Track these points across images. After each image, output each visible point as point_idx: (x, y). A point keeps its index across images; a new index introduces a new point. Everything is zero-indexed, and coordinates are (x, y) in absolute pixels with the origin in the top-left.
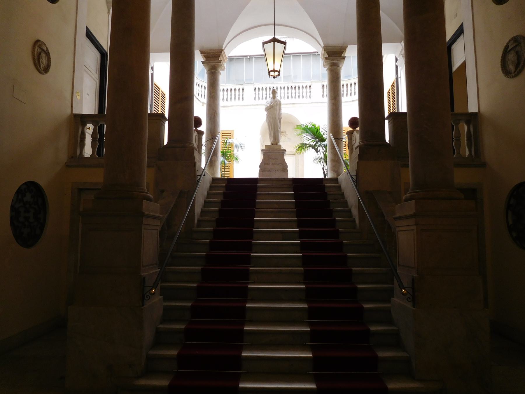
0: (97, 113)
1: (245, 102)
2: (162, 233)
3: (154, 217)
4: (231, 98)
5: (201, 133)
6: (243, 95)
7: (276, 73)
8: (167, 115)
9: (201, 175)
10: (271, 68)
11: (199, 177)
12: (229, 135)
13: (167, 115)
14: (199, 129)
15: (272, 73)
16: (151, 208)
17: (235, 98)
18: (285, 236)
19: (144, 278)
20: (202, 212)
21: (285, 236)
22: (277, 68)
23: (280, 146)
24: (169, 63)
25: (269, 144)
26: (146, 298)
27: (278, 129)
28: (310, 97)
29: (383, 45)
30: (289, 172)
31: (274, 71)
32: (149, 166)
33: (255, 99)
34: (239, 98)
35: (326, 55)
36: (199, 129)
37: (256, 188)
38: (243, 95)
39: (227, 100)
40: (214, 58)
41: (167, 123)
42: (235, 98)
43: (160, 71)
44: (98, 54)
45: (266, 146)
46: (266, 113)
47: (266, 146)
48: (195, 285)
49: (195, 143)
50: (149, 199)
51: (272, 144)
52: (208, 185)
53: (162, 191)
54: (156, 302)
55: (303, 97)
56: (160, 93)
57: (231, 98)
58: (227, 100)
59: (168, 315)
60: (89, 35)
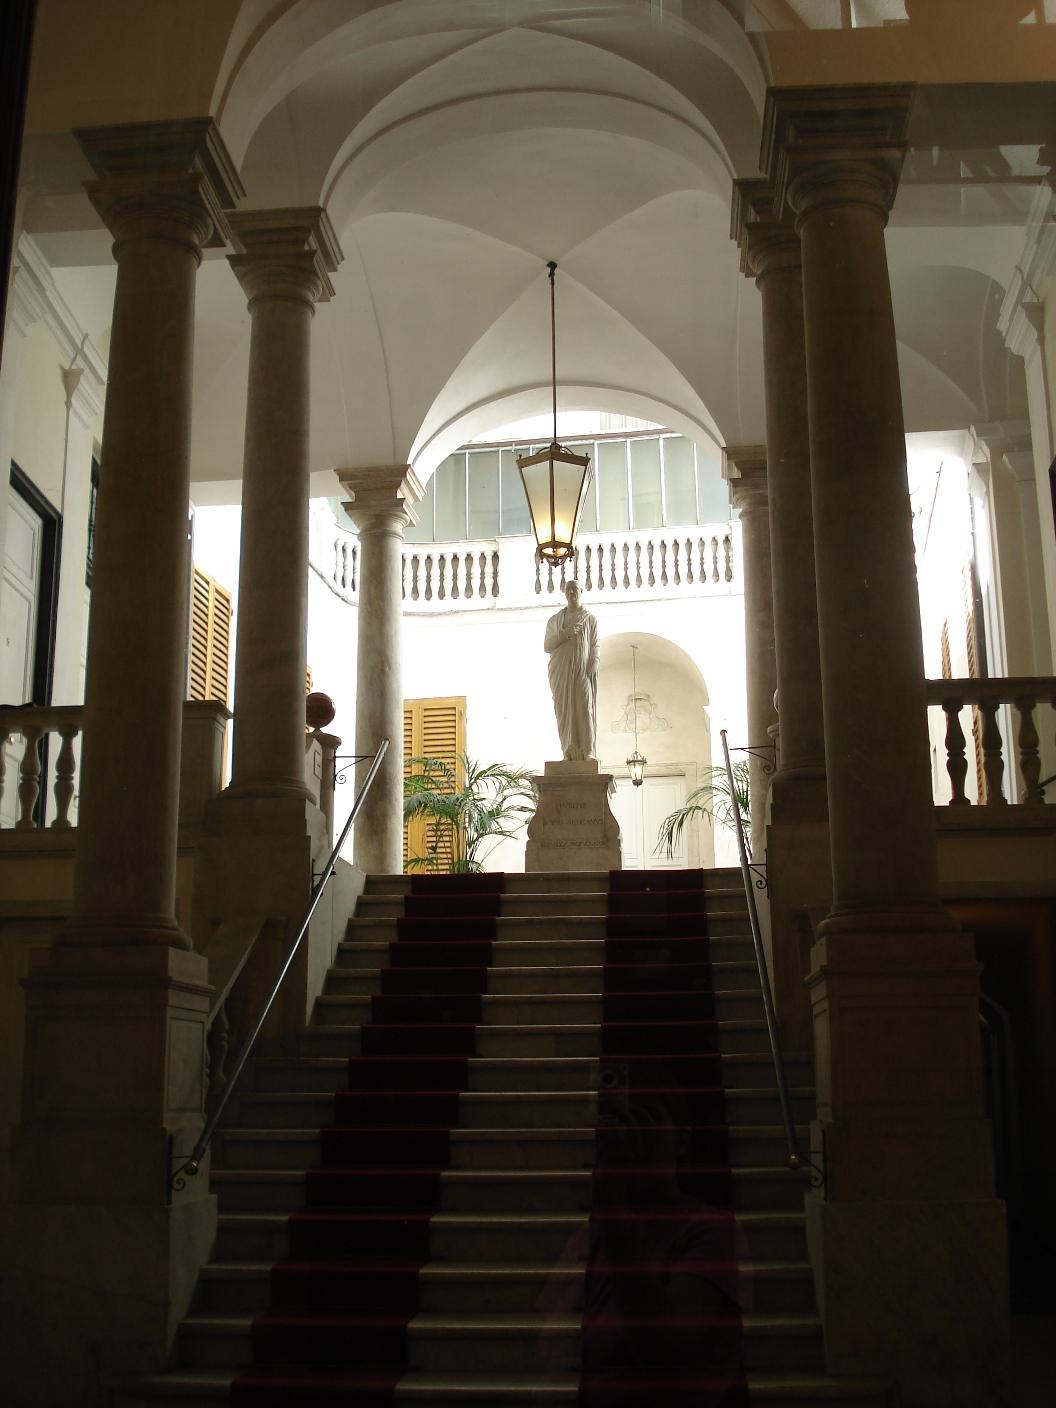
0: (28, 700)
1: (502, 600)
2: (213, 1039)
3: (193, 990)
4: (455, 589)
5: (331, 743)
6: (495, 574)
7: (562, 551)
8: (231, 707)
9: (324, 874)
10: (545, 537)
11: (317, 879)
12: (446, 717)
13: (231, 707)
14: (325, 730)
15: (549, 551)
16: (187, 965)
17: (469, 588)
18: (564, 1041)
19: (171, 1139)
20: (331, 981)
21: (564, 1041)
22: (563, 536)
23: (595, 763)
24: (239, 508)
25: (558, 756)
26: (176, 1186)
27: (585, 706)
28: (495, 590)
29: (907, 435)
30: (625, 847)
31: (555, 544)
32: (183, 851)
33: (538, 589)
34: (482, 587)
35: (737, 474)
36: (325, 730)
37: (496, 907)
38: (495, 574)
39: (442, 595)
40: (376, 497)
41: (230, 722)
42: (469, 588)
43: (215, 537)
44: (36, 522)
45: (547, 764)
46: (548, 657)
47: (547, 764)
48: (302, 1173)
49: (310, 780)
50: (182, 946)
51: (568, 754)
52: (348, 907)
53: (216, 923)
54: (196, 1203)
55: (703, 577)
56: (212, 596)
57: (455, 589)
58: (442, 595)
59: (229, 1242)
60: (21, 483)
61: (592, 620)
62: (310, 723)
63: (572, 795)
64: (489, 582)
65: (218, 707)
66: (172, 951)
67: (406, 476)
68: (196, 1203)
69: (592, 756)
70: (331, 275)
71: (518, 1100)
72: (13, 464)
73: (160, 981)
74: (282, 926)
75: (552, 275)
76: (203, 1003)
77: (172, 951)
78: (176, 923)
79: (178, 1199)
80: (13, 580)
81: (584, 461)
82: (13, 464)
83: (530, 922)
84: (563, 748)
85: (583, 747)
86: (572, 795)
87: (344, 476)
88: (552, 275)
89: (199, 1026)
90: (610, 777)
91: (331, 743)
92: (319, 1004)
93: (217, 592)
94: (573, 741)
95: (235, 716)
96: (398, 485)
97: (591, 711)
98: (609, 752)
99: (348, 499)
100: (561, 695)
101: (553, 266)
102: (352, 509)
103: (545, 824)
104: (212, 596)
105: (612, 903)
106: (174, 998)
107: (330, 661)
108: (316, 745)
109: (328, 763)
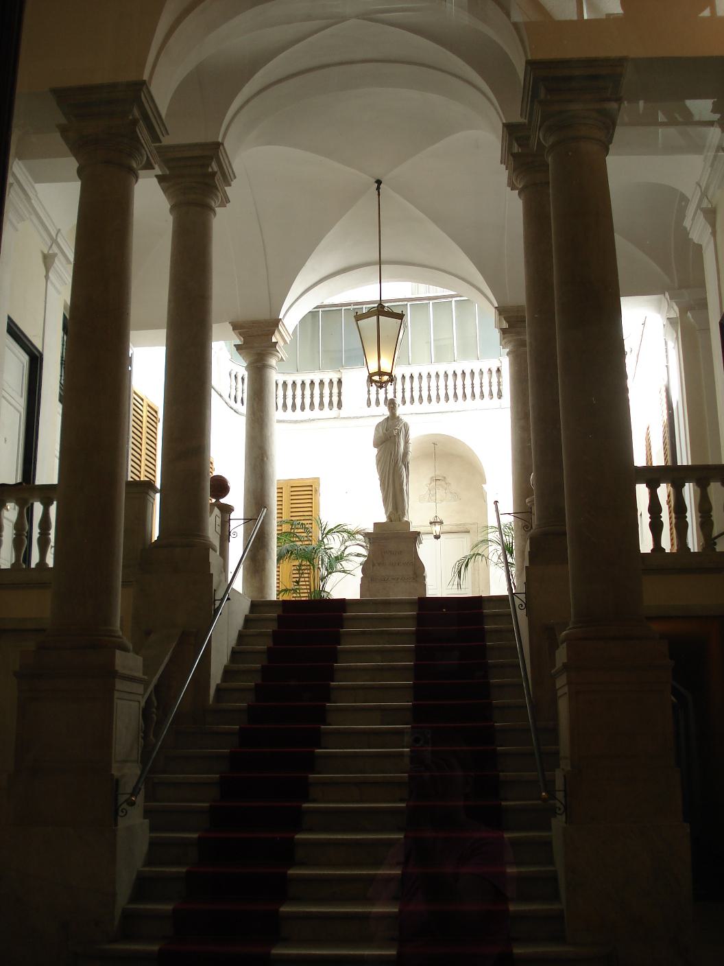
1: (344, 412)
2: (146, 713)
3: (132, 679)
4: (312, 404)
5: (227, 510)
6: (340, 394)
7: (386, 378)
8: (158, 485)
9: (222, 600)
10: (374, 369)
11: (217, 603)
12: (306, 492)
13: (158, 485)
14: (223, 501)
15: (376, 378)
16: (128, 662)
17: (321, 404)
18: (387, 714)
19: (117, 781)
20: (227, 673)
21: (387, 714)
22: (386, 368)
23: (408, 523)
24: (164, 348)
25: (383, 519)
26: (121, 814)
27: (401, 485)
28: (340, 405)
29: (622, 299)
30: (428, 581)
31: (380, 373)
32: (125, 584)
33: (369, 404)
34: (331, 403)
35: (505, 325)
36: (223, 501)
37: (340, 622)
38: (340, 394)
39: (303, 408)
40: (258, 341)
41: (158, 495)
42: (321, 404)
43: (147, 368)
44: (25, 358)
45: (375, 524)
46: (375, 451)
47: (375, 524)
48: (207, 805)
49: (213, 535)
50: (125, 649)
51: (389, 517)
53: (148, 633)
54: (134, 825)
55: (482, 396)
56: (145, 409)
57: (312, 404)
58: (303, 408)
59: (157, 852)
60: (14, 332)
61: (406, 426)
62: (213, 496)
63: (392, 546)
64: (335, 399)
65: (149, 485)
66: (118, 652)
67: (278, 327)
68: (134, 825)
69: (406, 519)
70: (227, 188)
71: (355, 755)
72: (9, 318)
73: (109, 673)
74: (194, 635)
75: (378, 188)
76: (139, 688)
77: (118, 652)
78: (120, 633)
79: (122, 823)
80: (9, 398)
81: (400, 316)
82: (9, 318)
83: (363, 633)
84: (386, 513)
85: (400, 513)
86: (392, 546)
87: (236, 327)
88: (378, 188)
89: (137, 704)
90: (418, 533)
91: (227, 510)
92: (218, 689)
93: (149, 406)
94: (393, 508)
95: (161, 491)
96: (273, 333)
97: (405, 488)
98: (417, 516)
99: (238, 342)
100: (385, 477)
101: (379, 182)
102: (241, 349)
103: (374, 565)
104: (145, 409)
105: (420, 620)
106: (119, 685)
107: (226, 454)
108: (217, 511)
109: (225, 523)
